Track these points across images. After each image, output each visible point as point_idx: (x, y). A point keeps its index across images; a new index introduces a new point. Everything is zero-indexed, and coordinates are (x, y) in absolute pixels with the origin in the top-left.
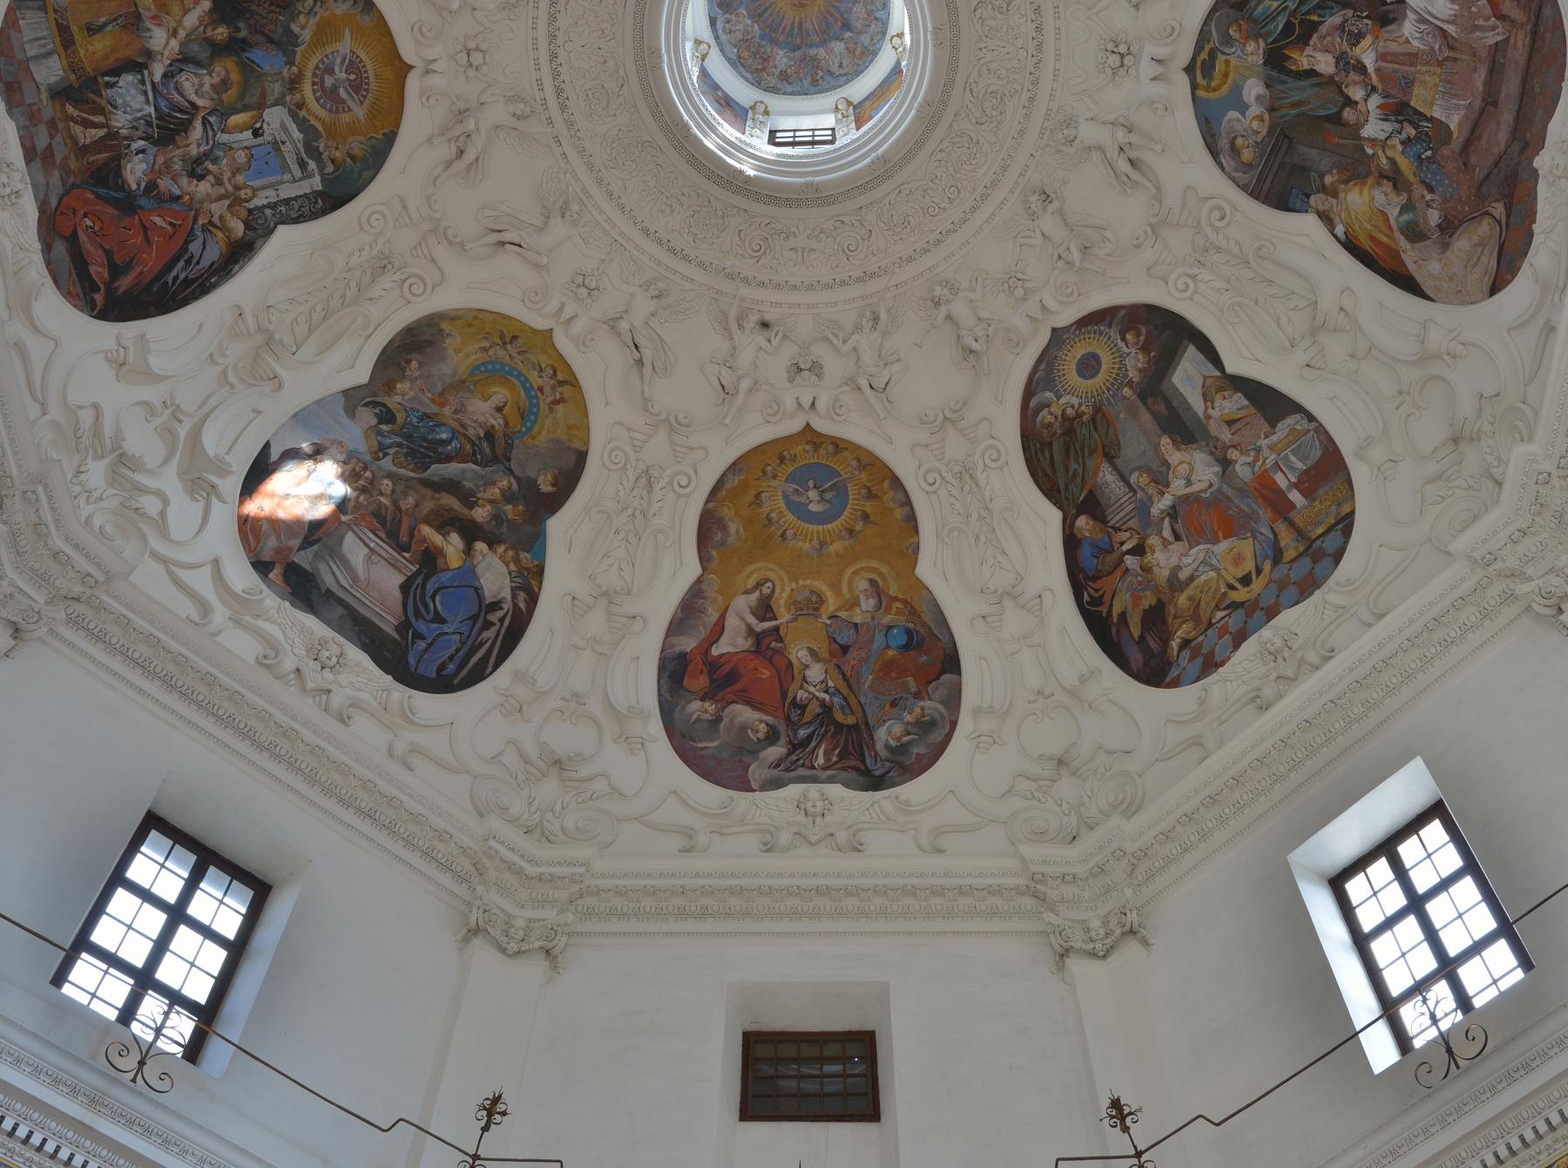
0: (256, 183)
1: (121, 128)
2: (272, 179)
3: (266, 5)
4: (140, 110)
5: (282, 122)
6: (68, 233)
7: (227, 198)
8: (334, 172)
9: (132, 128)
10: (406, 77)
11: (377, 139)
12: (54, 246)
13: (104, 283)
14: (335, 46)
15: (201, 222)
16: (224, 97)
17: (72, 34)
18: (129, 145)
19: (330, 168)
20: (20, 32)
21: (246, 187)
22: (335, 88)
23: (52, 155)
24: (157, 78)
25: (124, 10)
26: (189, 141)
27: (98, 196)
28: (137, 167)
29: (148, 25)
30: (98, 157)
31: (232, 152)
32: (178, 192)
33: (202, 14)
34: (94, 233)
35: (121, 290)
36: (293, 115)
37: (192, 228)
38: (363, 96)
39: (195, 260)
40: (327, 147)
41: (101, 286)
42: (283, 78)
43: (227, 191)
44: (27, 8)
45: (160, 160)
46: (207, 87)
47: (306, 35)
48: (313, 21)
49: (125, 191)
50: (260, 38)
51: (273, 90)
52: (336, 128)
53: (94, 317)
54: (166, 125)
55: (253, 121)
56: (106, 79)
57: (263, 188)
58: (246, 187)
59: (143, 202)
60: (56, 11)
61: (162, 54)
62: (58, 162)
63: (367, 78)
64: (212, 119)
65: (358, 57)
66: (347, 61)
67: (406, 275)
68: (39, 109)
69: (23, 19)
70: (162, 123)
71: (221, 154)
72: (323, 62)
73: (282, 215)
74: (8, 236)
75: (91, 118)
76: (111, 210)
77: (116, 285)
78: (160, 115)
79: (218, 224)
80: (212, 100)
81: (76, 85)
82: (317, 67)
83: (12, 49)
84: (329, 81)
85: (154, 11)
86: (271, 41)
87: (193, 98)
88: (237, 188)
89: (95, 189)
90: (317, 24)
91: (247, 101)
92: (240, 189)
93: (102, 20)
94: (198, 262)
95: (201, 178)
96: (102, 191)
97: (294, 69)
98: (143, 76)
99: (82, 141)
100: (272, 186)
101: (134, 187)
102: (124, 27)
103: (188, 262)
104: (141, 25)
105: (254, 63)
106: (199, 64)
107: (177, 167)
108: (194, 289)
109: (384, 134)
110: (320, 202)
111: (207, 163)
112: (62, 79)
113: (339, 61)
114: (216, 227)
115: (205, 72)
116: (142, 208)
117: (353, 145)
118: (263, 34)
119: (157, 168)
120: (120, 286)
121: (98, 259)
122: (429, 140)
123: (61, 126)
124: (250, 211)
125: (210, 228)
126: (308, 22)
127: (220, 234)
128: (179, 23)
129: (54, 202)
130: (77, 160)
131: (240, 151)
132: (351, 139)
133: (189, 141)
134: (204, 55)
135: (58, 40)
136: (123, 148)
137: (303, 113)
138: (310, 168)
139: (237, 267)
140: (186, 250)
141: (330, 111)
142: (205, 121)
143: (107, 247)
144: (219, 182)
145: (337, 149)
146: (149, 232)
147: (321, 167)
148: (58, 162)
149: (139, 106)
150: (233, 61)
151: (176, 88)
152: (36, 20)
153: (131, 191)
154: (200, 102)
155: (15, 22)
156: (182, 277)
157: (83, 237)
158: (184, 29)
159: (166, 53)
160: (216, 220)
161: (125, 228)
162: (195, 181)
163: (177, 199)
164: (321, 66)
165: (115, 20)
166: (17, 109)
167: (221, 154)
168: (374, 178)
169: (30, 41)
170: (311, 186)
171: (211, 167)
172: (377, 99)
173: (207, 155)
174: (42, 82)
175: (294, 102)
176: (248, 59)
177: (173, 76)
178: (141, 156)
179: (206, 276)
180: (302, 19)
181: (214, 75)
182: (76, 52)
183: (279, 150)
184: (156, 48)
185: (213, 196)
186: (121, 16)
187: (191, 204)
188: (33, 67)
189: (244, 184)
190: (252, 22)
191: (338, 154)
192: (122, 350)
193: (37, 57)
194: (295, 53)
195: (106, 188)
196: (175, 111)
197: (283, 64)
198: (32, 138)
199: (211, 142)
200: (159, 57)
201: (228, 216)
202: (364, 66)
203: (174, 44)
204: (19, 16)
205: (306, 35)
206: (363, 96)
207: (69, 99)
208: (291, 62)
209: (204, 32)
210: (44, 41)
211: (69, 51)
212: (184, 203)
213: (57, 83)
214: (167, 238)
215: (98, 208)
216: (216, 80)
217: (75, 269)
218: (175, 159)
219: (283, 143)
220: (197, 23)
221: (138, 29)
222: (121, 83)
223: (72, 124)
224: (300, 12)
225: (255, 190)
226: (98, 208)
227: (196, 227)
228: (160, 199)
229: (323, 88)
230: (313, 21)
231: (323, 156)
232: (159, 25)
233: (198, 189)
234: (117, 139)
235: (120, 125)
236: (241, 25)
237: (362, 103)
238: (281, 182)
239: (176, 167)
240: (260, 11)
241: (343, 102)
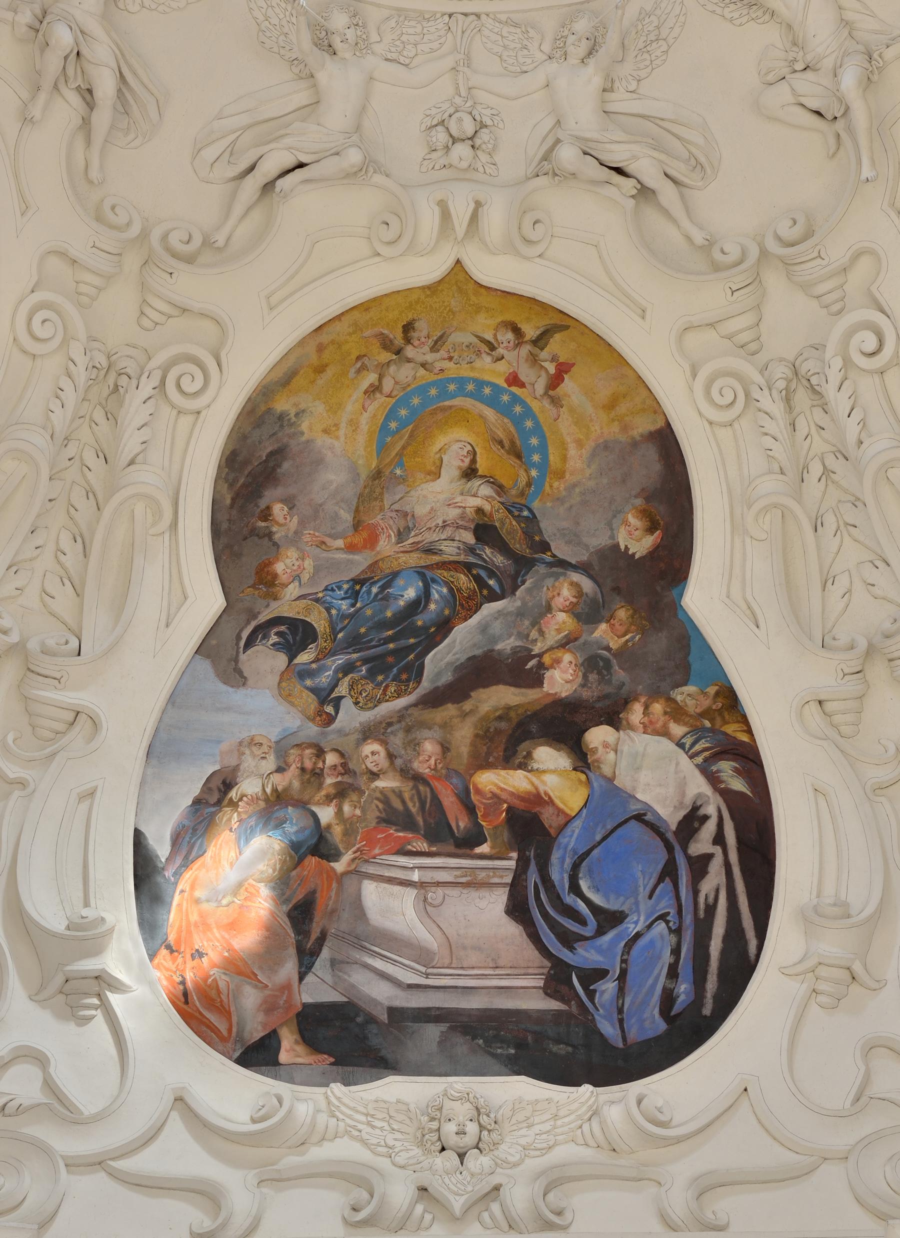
122: (27, 120)
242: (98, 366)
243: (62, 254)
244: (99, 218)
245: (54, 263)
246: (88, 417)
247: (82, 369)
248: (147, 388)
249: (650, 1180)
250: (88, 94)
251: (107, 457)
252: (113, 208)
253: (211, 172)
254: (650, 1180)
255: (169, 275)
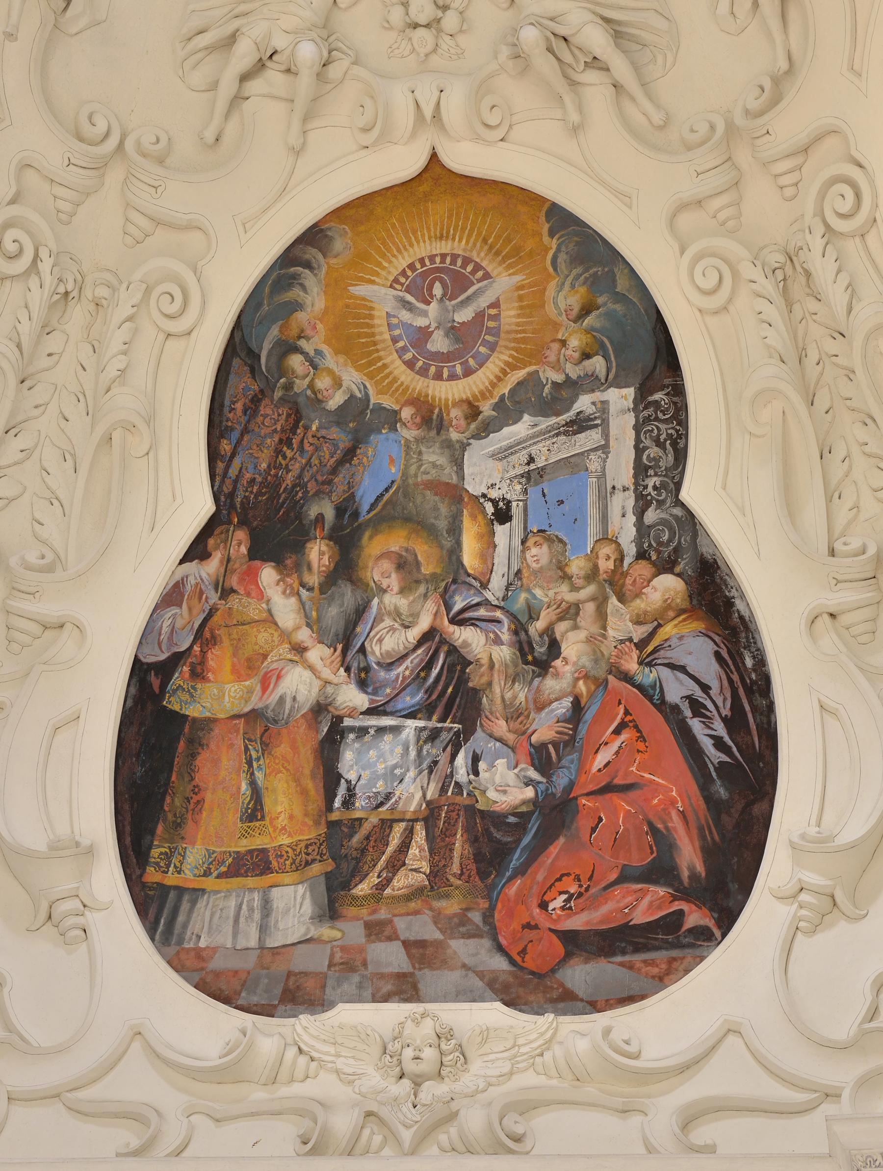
0: (592, 532)
1: (424, 795)
2: (591, 497)
3: (289, 454)
4: (406, 749)
5: (493, 456)
6: (559, 949)
7: (606, 599)
8: (606, 357)
9: (430, 772)
10: (450, 170)
11: (558, 250)
12: (569, 985)
13: (675, 898)
14: (380, 321)
15: (631, 665)
16: (427, 569)
17: (251, 852)
18: (457, 783)
19: (598, 364)
20: (215, 950)
21: (593, 557)
22: (454, 331)
23: (422, 944)
24: (361, 700)
25: (239, 742)
26: (485, 661)
27: (521, 871)
28: (498, 779)
29: (272, 699)
30: (456, 854)
31: (525, 573)
32: (567, 702)
33: (280, 589)
34: (580, 895)
35: (700, 868)
36: (486, 429)
37: (640, 688)
38: (474, 272)
39: (699, 693)
40: (557, 366)
41: (677, 906)
42: (418, 440)
43: (593, 599)
44: (185, 926)
45: (501, 727)
46: (403, 603)
47: (351, 378)
48: (330, 361)
49: (529, 814)
50: (339, 480)
51: (434, 465)
52: (524, 340)
53: (724, 936)
54: (445, 700)
55: (480, 518)
56: (337, 803)
57: (604, 518)
58: (593, 557)
59: (561, 780)
60: (207, 873)
61: (327, 682)
62: (438, 936)
63: (443, 256)
64: (459, 603)
65: (403, 273)
66: (409, 298)
67: (818, 220)
68: (343, 949)
69: (199, 937)
70: (439, 710)
71: (523, 596)
72: (404, 349)
73: (664, 485)
74: (511, 1073)
75: (390, 849)
76: (554, 850)
77: (685, 874)
78: (426, 710)
79: (649, 628)
80: (426, 596)
81: (330, 866)
82: (410, 364)
83: (236, 972)
84: (439, 343)
85: (253, 683)
86: (350, 454)
87: (413, 635)
88: (592, 575)
89: (508, 874)
90: (337, 352)
91: (442, 524)
92: (596, 568)
93: (244, 786)
94: (705, 688)
95: (554, 648)
96: (516, 859)
97: (406, 413)
98: (352, 729)
99: (420, 879)
100: (605, 494)
101: (529, 793)
102: (266, 746)
103: (697, 708)
104: (270, 714)
105: (382, 495)
106: (360, 611)
107: (521, 694)
108: (754, 709)
109: (552, 234)
110: (658, 396)
111: (532, 630)
112: (312, 889)
113: (405, 316)
114: (652, 635)
115: (376, 601)
116: (571, 785)
117: (562, 306)
118: (334, 471)
119: (511, 738)
120: (691, 869)
121: (629, 899)
122: (576, 130)
123: (383, 914)
124: (641, 555)
125: (650, 648)
126: (330, 372)
127: (668, 630)
128: (285, 636)
129: (500, 963)
130: (447, 896)
131: (528, 555)
132: (550, 310)
133: (485, 661)
134: (348, 596)
135: (251, 881)
136: (458, 799)
137: (487, 409)
138: (590, 410)
139: (739, 605)
140: (676, 708)
141: (493, 347)
142: (458, 620)
143: (613, 876)
144: (571, 612)
145: (563, 343)
146: (618, 781)
147: (592, 383)
148: (438, 936)
149: (399, 750)
150: (371, 538)
151: (389, 666)
152: (208, 914)
153: (535, 802)
154: (424, 624)
155: (199, 954)
156: (720, 729)
157: (576, 923)
158: (297, 628)
159: (327, 673)
160: (639, 632)
161: (593, 830)
162: (558, 663)
163: (577, 707)
164: (408, 356)
165: (250, 763)
166: (328, 990)
167: (523, 596)
168: (632, 270)
169: (235, 934)
170: (624, 412)
171: (540, 625)
172: (485, 241)
173: (519, 629)
174: (303, 930)
175: (463, 422)
176: (373, 506)
177: (367, 669)
178: (482, 766)
179: (735, 677)
180: (323, 383)
181: (385, 583)
182: (279, 852)
183: (541, 472)
184: (315, 691)
185: (595, 629)
186: (247, 749)
187: (595, 680)
188: (275, 941)
189: (589, 560)
190: (312, 487)
191: (575, 343)
192: (804, 897)
193: (263, 929)
194: (379, 408)
195: (512, 850)
196: (425, 679)
197: (392, 436)
198: (382, 976)
199: (498, 614)
200: (329, 689)
201: (639, 604)
202: (422, 261)
203: (317, 654)
204: (192, 945)
205: (351, 378)
206: (474, 272)
207: (347, 886)
208: (392, 419)
209: (310, 589)
210: (244, 907)
211: (274, 864)
212: (591, 695)
213: (315, 902)
214: (641, 746)
215: (540, 877)
216: (394, 581)
217: (624, 953)
218: (508, 695)
219: (531, 460)
220: (293, 600)
221: (276, 722)
222: (352, 776)
223: (388, 891)
224: (311, 386)
225: (605, 538)
226: (540, 877)
227: (639, 679)
228: (566, 744)
229: (447, 357)
230: (330, 361)
231: (573, 376)
232: (279, 677)
233: (573, 658)
234: (440, 808)
235: (418, 795)
236: (313, 512)
237: (487, 276)
238: (602, 477)
239: (522, 697)
240: (296, 468)
241: (480, 316)
242: (777, 265)
243: (683, 207)
244: (689, 147)
245: (686, 221)
246: (807, 315)
247: (762, 279)
248: (817, 243)
249: (634, 1110)
250: (595, 63)
251: (842, 331)
252: (692, 131)
253: (737, 20)
254: (634, 1110)
255: (768, 135)
